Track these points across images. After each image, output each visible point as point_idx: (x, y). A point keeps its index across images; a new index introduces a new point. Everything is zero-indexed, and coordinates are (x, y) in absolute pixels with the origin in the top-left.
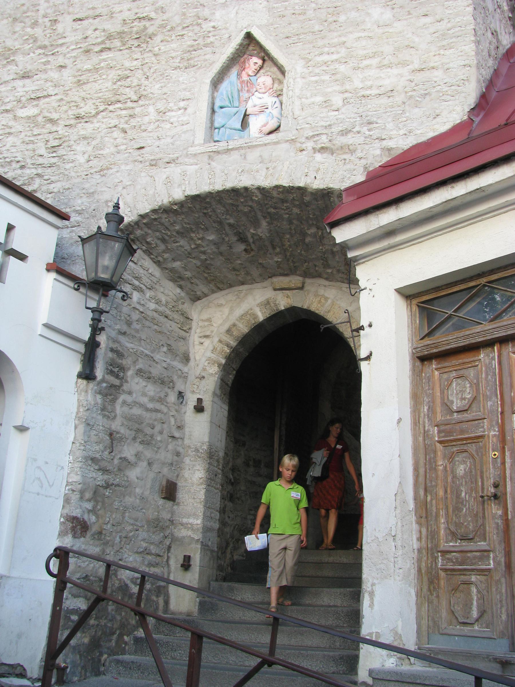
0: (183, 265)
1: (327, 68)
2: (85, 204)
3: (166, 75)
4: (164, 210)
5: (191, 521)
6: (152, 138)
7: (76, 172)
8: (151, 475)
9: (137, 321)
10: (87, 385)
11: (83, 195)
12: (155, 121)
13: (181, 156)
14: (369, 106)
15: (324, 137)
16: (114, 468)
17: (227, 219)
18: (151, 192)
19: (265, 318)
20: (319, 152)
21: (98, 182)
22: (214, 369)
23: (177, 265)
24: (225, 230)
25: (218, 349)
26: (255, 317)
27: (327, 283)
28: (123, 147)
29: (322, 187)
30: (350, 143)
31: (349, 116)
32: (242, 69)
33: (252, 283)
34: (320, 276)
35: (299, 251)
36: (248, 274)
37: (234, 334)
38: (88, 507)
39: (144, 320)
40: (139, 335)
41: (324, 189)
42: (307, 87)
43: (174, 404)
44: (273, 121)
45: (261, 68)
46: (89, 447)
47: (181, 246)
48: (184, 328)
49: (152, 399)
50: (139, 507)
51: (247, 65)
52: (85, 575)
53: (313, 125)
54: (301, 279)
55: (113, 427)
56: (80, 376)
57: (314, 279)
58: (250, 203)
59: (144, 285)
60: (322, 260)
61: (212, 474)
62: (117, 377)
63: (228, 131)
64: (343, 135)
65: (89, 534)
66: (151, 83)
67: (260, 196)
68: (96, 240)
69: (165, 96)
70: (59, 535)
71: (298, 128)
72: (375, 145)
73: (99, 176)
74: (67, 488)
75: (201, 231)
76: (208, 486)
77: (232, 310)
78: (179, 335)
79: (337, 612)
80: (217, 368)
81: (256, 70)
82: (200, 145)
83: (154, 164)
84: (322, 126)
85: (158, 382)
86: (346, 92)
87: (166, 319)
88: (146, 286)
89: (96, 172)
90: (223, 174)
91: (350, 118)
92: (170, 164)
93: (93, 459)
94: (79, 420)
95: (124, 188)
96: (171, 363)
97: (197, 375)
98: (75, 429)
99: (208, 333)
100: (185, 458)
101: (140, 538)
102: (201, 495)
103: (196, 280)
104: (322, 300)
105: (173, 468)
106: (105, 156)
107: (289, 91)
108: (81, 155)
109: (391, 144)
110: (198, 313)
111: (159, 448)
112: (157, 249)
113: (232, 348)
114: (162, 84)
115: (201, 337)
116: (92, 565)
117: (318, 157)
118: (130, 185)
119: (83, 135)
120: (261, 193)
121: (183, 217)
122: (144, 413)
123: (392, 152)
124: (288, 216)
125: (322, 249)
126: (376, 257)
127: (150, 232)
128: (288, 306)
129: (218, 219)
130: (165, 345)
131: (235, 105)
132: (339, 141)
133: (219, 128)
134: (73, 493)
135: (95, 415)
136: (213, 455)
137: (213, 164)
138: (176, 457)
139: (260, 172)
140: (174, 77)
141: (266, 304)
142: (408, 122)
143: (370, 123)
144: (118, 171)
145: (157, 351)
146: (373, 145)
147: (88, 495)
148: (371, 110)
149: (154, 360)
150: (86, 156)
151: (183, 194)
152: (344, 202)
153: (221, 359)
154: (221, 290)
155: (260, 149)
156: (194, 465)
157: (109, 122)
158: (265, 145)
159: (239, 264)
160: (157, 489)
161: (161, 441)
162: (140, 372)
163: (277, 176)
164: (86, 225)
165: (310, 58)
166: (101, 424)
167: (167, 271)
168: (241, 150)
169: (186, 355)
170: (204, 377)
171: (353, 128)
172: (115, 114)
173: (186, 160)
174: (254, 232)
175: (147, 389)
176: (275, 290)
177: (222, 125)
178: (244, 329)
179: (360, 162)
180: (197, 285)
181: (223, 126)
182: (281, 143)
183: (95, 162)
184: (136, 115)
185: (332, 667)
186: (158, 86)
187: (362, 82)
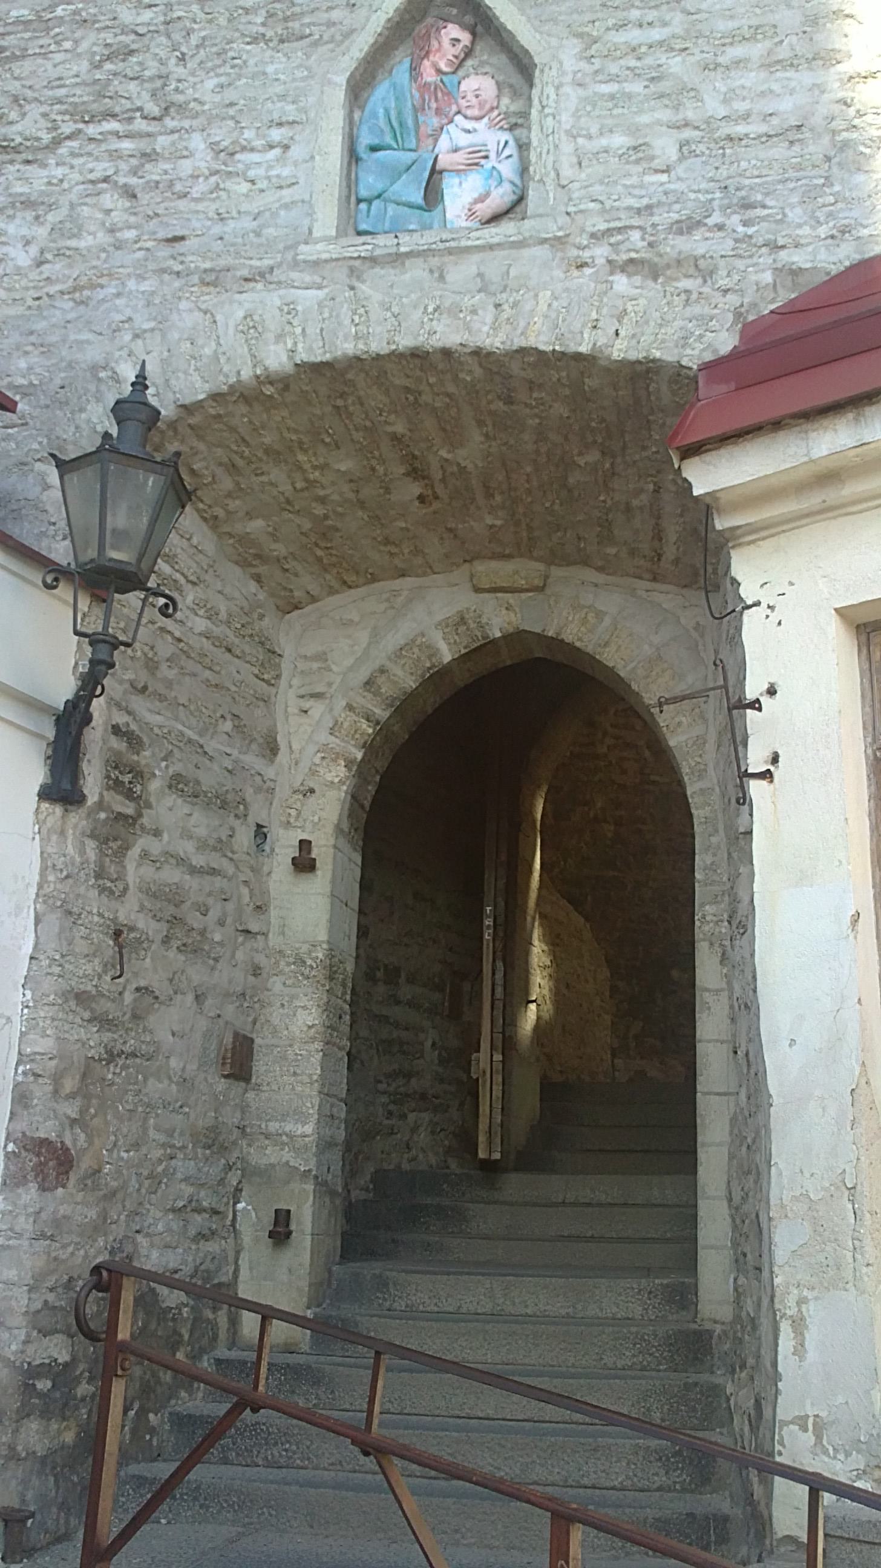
0: (270, 529)
1: (638, 64)
2: (38, 370)
3: (231, 54)
4: (242, 394)
5: (289, 1127)
6: (201, 216)
7: (9, 290)
8: (203, 1024)
9: (168, 660)
11: (29, 348)
12: (207, 173)
13: (280, 265)
14: (742, 163)
15: (635, 235)
16: (125, 1014)
17: (389, 424)
18: (207, 351)
20: (622, 271)
21: (69, 317)
22: (338, 772)
23: (256, 526)
24: (378, 448)
26: (433, 652)
27: (601, 578)
28: (130, 234)
29: (633, 355)
30: (701, 251)
31: (696, 188)
32: (423, 53)
33: (424, 574)
34: (585, 562)
35: (547, 505)
36: (417, 551)
37: (383, 690)
38: (69, 1112)
39: (184, 657)
40: (173, 694)
41: (639, 362)
42: (589, 108)
43: (248, 854)
44: (501, 190)
45: (469, 53)
46: (71, 967)
47: (271, 484)
48: (266, 677)
49: (202, 846)
50: (177, 1101)
51: (435, 44)
52: (66, 1277)
53: (608, 204)
54: (541, 566)
55: (122, 918)
56: (46, 794)
57: (570, 568)
58: (451, 388)
59: (183, 574)
60: (600, 526)
61: (334, 1015)
62: (129, 795)
63: (391, 209)
64: (680, 232)
65: (73, 1177)
66: (193, 74)
67: (478, 372)
68: (99, 465)
69: (231, 112)
70: (5, 1183)
71: (571, 209)
72: (761, 260)
73: (71, 304)
74: (21, 1069)
75: (321, 449)
76: (327, 1043)
77: (376, 636)
78: (256, 692)
79: (643, 1337)
80: (344, 769)
81: (456, 57)
82: (326, 239)
83: (212, 280)
84: (629, 208)
85: (215, 804)
86: (686, 125)
87: (227, 654)
88: (186, 577)
89: (62, 293)
90: (389, 314)
91: (699, 191)
92: (252, 284)
93: (82, 998)
94: (45, 902)
95: (136, 336)
96: (242, 757)
97: (297, 784)
98: (36, 925)
99: (319, 689)
100: (271, 980)
101: (179, 1176)
102: (313, 1065)
103: (295, 563)
104: (612, 624)
105: (246, 1005)
106: (84, 252)
107: (546, 116)
108: (20, 246)
109: (799, 259)
110: (291, 638)
111: (216, 960)
112: (214, 489)
113: (378, 723)
114: (223, 79)
115: (302, 697)
116: (82, 1252)
117: (621, 283)
118: (152, 330)
119: (21, 194)
120: (480, 365)
121: (283, 414)
122: (188, 877)
123: (800, 280)
124: (537, 421)
125: (604, 501)
126: (784, 531)
127: (202, 447)
129: (368, 424)
130: (229, 717)
131: (407, 146)
132: (673, 247)
133: (369, 201)
134: (35, 1081)
135: (82, 890)
136: (335, 972)
137: (364, 288)
138: (253, 978)
139: (480, 312)
140: (251, 62)
141: (457, 624)
142: (840, 205)
143: (747, 206)
144: (118, 295)
145: (211, 731)
146: (755, 260)
147: (69, 1084)
148: (748, 174)
149: (206, 753)
150: (34, 250)
151: (290, 358)
152: (700, 397)
153: (353, 750)
154: (350, 587)
155: (476, 257)
156: (293, 997)
157: (90, 166)
159: (402, 529)
160: (212, 1056)
161: (221, 944)
162: (176, 783)
163: (522, 324)
164: (42, 423)
165: (595, 33)
166: (95, 911)
167: (231, 541)
168: (430, 259)
169: (271, 740)
170: (312, 791)
171: (706, 217)
172: (104, 147)
173: (294, 275)
174: (449, 456)
175: (193, 820)
176: (477, 590)
177: (376, 194)
179: (724, 300)
180: (296, 575)
181: (379, 196)
182: (529, 246)
183: (58, 267)
184: (158, 154)
185: (657, 1474)
186: (210, 84)
187: (726, 101)
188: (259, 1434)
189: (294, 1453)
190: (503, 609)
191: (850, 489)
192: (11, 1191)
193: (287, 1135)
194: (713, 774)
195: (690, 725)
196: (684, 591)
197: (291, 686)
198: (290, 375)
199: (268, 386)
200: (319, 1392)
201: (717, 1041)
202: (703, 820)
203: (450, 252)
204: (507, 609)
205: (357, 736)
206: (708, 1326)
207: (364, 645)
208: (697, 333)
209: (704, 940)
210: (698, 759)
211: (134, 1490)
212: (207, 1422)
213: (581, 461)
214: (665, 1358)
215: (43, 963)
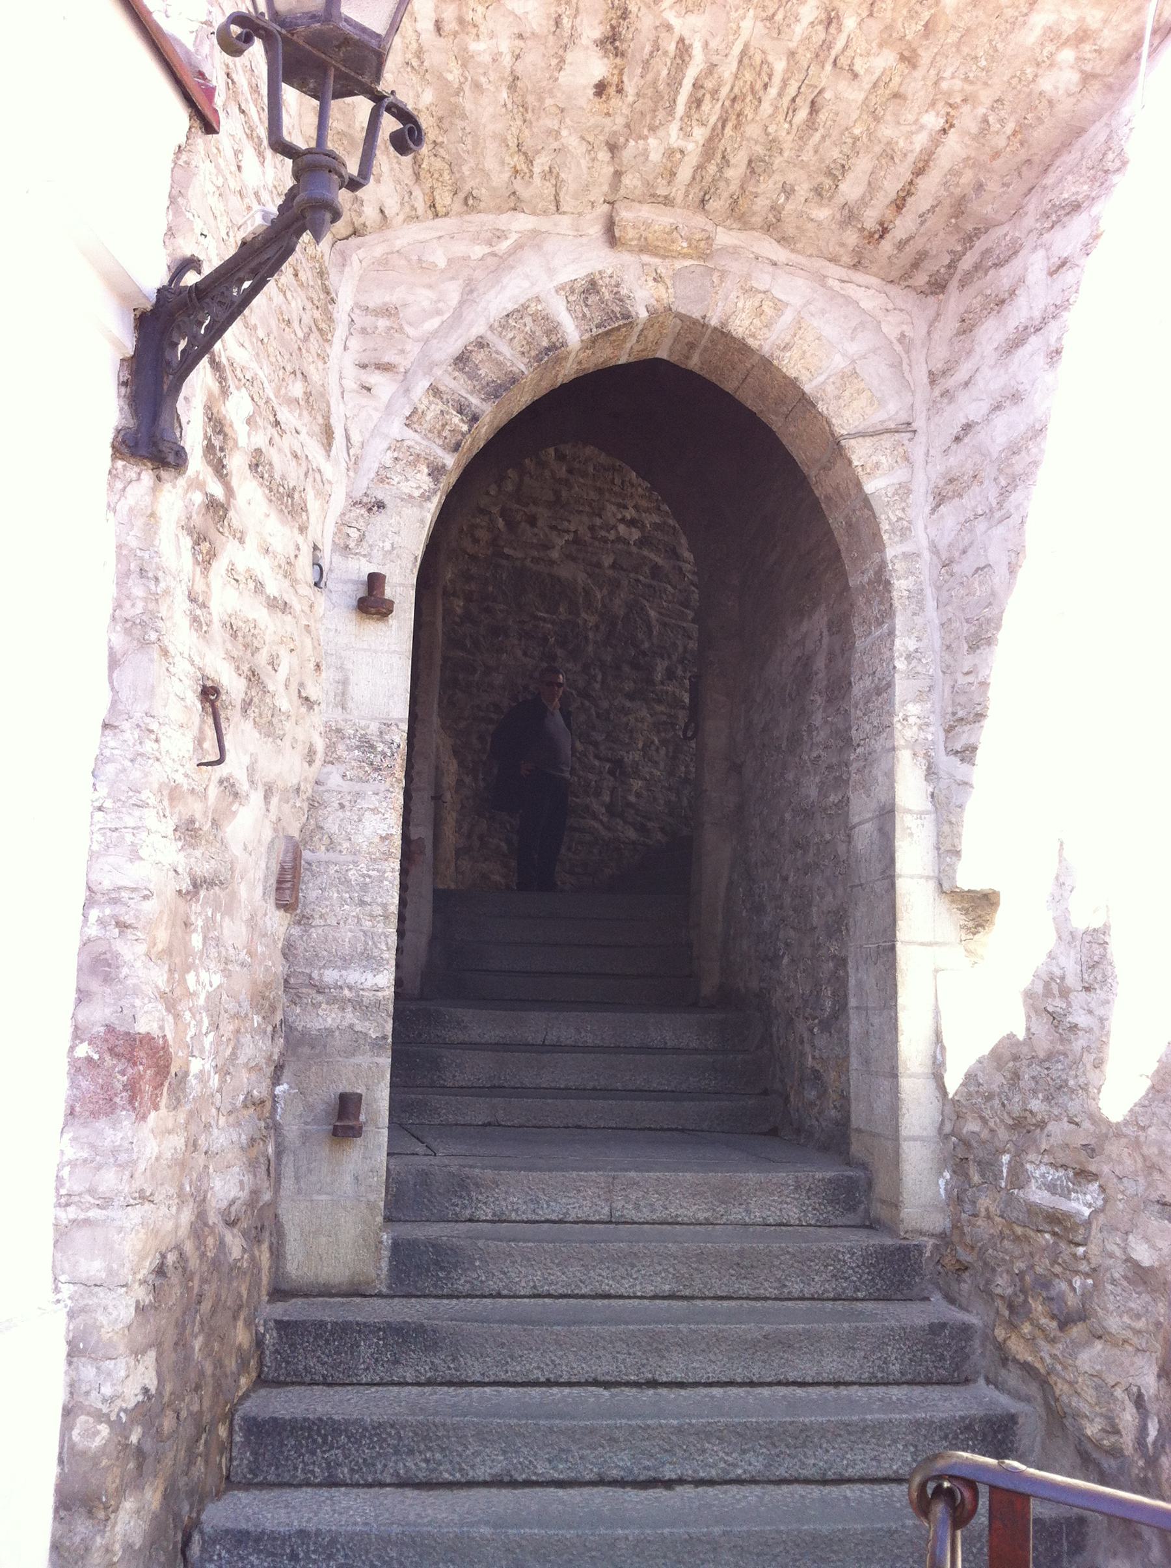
5: (354, 976)
10: (154, 490)
25: (430, 415)
37: (482, 372)
70: (71, 1113)
80: (428, 479)
97: (358, 495)
170: (381, 505)
188: (385, 1440)
189: (440, 1463)
190: (650, 279)
192: (85, 1125)
193: (350, 988)
196: (889, 288)
200: (437, 1361)
201: (922, 877)
202: (906, 594)
204: (655, 280)
205: (446, 433)
209: (906, 747)
210: (900, 514)
211: (228, 1551)
212: (302, 1428)
214: (863, 1283)
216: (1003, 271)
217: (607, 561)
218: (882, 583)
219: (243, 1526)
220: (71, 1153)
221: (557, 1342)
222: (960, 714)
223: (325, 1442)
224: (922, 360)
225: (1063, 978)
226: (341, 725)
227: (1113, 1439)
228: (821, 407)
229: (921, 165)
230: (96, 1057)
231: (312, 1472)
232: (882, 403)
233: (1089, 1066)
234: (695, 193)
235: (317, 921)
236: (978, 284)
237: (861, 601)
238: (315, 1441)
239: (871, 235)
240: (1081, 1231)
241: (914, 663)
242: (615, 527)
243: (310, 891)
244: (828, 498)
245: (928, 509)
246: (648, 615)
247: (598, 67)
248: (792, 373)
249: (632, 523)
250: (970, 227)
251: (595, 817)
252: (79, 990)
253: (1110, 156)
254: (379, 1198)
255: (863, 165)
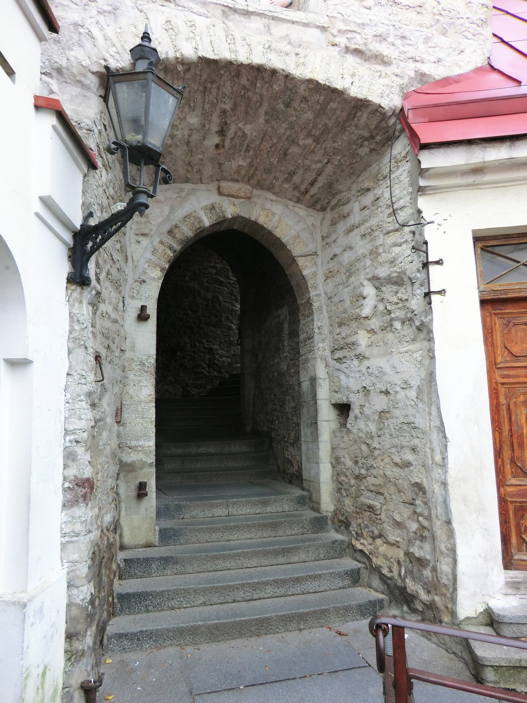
5: (141, 443)
19: (211, 224)
20: (352, 53)
26: (200, 221)
27: (273, 197)
29: (360, 96)
33: (197, 183)
37: (177, 236)
56: (71, 280)
70: (64, 505)
74: (68, 438)
77: (172, 209)
80: (160, 272)
97: (136, 278)
99: (146, 231)
109: (426, 68)
115: (137, 235)
118: (110, 12)
128: (236, 215)
155: (286, 26)
158: (293, 22)
170: (144, 281)
174: (243, 127)
178: (188, 232)
189: (182, 602)
191: (488, 177)
194: (321, 288)
195: (311, 267)
196: (308, 209)
197: (131, 229)
198: (194, 62)
199: (180, 65)
200: (178, 567)
201: (324, 399)
203: (274, 18)
206: (325, 514)
207: (167, 213)
208: (387, 92)
209: (318, 358)
210: (314, 282)
211: (117, 640)
212: (137, 595)
213: (301, 143)
215: (76, 377)
216: (345, 207)
217: (205, 280)
218: (309, 303)
219: (121, 632)
220: (65, 519)
221: (216, 558)
222: (336, 347)
223: (144, 599)
224: (319, 232)
225: (371, 433)
226: (133, 357)
227: (391, 574)
228: (288, 247)
229: (319, 173)
230: (72, 487)
231: (141, 609)
232: (307, 246)
233: (380, 460)
234: (246, 179)
235: (128, 425)
236: (337, 210)
237: (302, 308)
238: (141, 599)
239: (303, 193)
240: (379, 511)
241: (320, 330)
242: (207, 269)
243: (125, 415)
244: (290, 275)
245: (323, 280)
246: (219, 298)
247: (216, 140)
248: (279, 236)
249: (213, 267)
250: (334, 192)
251: (204, 368)
252: (64, 465)
253: (380, 175)
254: (154, 515)
255: (300, 172)
